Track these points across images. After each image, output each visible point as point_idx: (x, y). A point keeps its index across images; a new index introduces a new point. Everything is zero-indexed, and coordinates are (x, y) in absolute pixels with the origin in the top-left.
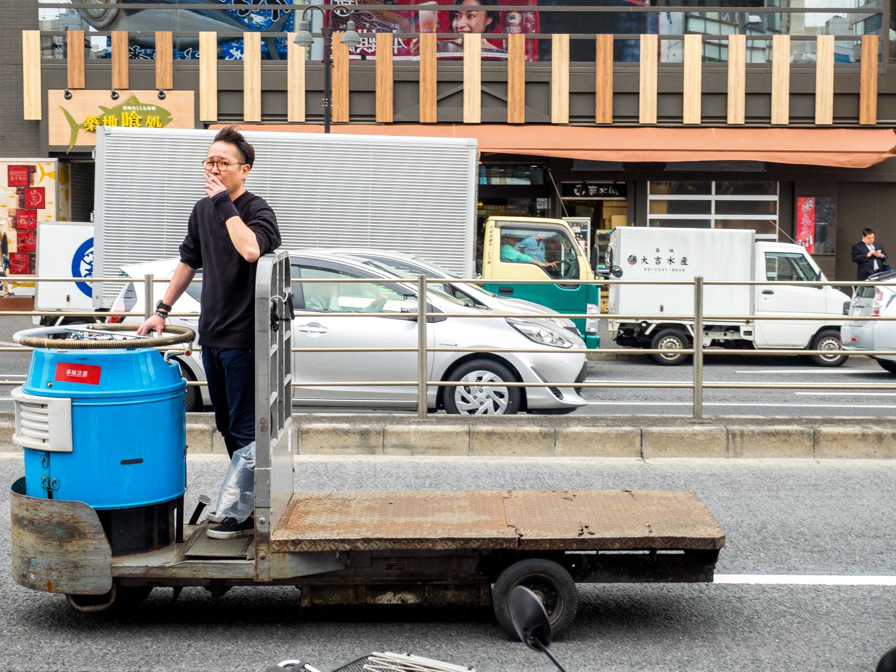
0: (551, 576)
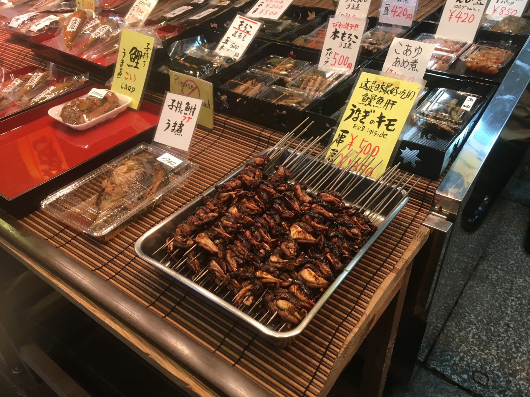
0: (207, 389)
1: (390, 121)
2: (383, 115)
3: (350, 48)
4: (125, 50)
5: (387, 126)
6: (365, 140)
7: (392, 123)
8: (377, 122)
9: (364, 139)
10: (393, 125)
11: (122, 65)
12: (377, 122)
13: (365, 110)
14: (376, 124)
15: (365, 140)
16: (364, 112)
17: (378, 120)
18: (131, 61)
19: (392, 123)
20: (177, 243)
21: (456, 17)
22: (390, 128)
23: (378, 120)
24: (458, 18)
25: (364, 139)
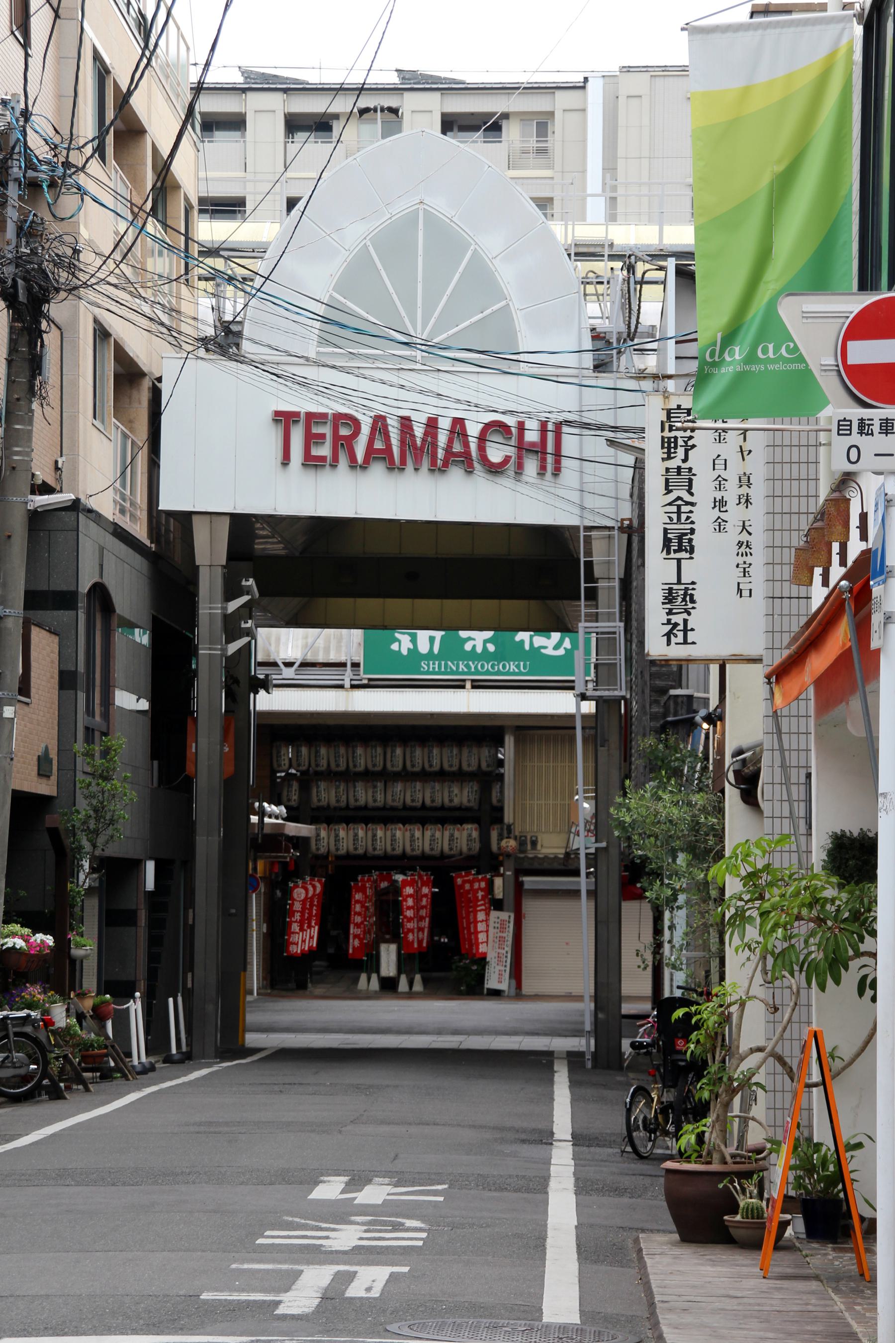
19: (690, 443)
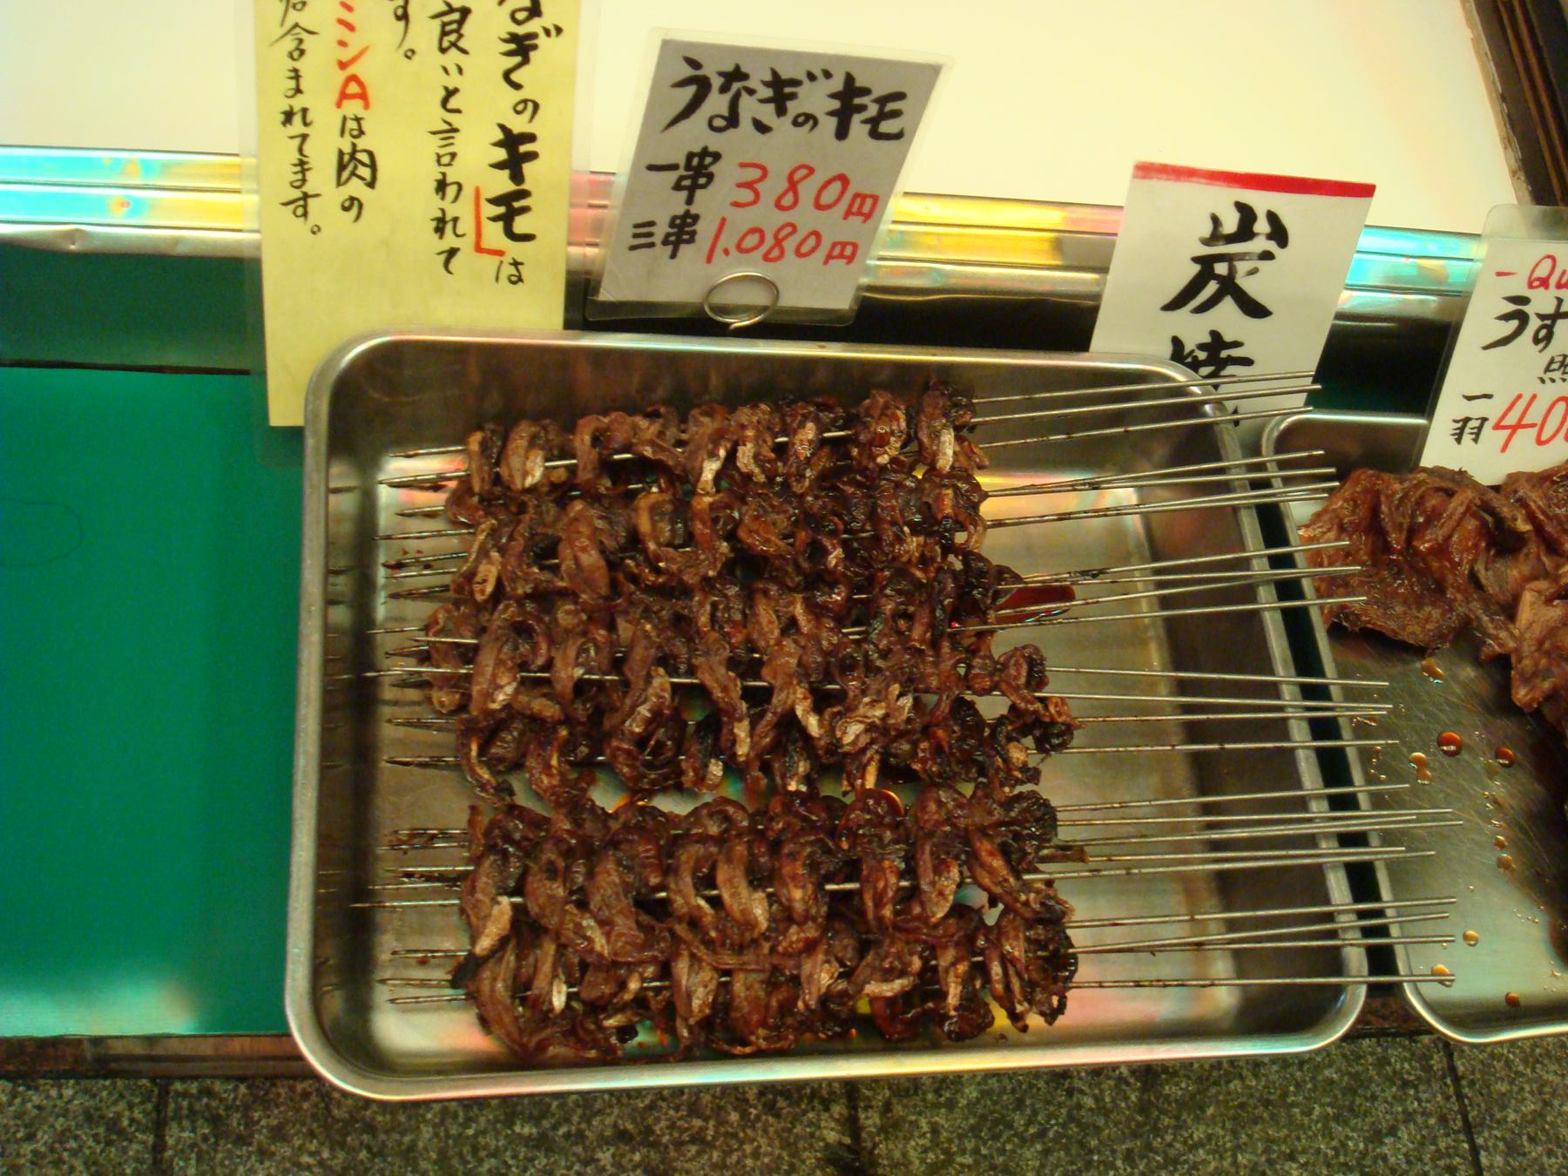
1: (882, 101)
2: (859, 83)
3: (1541, 346)
4: (349, 8)
5: (874, 122)
6: (520, 267)
7: (890, 106)
8: (832, 114)
9: (522, 264)
10: (896, 114)
11: (304, 181)
12: (832, 114)
13: (775, 73)
14: (829, 125)
15: (520, 267)
16: (766, 84)
17: (836, 104)
18: (358, 120)
19: (890, 106)
20: (955, 938)
21: (1497, 427)
22: (887, 126)
23: (836, 104)
24: (1507, 432)
25: (522, 264)
